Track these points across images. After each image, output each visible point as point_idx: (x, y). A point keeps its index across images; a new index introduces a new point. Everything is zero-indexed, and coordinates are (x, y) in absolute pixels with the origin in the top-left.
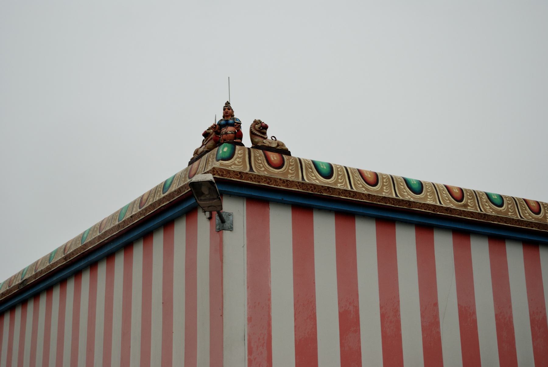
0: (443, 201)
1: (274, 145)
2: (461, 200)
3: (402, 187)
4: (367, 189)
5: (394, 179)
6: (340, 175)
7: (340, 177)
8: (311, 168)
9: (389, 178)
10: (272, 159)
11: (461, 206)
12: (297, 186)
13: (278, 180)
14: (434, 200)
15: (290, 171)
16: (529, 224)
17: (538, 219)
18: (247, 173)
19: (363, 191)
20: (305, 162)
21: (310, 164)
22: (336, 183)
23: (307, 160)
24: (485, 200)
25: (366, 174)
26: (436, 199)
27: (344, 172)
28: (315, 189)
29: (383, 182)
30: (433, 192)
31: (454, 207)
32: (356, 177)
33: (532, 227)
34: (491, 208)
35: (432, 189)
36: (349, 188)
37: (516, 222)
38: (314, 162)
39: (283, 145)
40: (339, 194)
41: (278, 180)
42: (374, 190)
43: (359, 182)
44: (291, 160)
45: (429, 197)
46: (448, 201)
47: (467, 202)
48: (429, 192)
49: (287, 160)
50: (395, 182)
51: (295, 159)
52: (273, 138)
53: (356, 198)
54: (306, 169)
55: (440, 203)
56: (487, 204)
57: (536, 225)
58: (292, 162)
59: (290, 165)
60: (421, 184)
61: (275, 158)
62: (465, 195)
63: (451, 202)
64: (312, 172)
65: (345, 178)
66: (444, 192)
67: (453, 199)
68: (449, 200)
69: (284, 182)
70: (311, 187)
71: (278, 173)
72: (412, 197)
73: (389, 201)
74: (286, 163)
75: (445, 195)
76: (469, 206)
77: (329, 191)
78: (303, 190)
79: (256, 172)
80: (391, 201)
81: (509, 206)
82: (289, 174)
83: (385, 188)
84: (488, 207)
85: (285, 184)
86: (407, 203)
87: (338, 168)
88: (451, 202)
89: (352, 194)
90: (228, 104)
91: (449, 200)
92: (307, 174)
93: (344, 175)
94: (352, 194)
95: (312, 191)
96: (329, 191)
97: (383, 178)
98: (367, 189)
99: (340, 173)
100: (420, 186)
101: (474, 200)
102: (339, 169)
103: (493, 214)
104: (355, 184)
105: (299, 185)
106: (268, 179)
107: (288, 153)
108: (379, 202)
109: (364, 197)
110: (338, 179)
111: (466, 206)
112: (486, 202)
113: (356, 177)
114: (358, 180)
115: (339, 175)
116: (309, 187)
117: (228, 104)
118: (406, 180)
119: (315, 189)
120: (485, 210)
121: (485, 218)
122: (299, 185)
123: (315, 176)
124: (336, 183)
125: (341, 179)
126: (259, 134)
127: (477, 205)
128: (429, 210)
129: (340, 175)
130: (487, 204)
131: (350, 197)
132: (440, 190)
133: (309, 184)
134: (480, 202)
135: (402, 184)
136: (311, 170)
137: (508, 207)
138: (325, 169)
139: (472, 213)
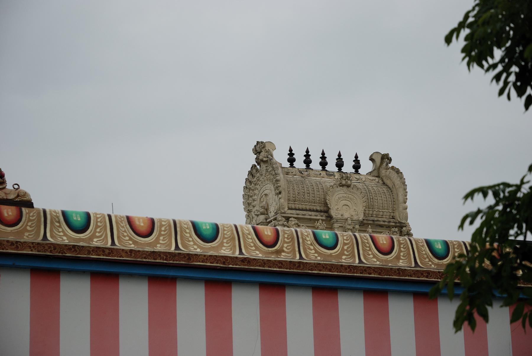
0: (246, 248)
3: (188, 235)
4: (135, 242)
5: (178, 225)
6: (99, 227)
7: (98, 230)
8: (59, 222)
9: (170, 225)
10: (6, 215)
11: (272, 253)
12: (30, 247)
13: (5, 243)
14: (233, 249)
15: (28, 228)
16: (365, 270)
18: (38, 244)
19: (259, 255)
20: (51, 214)
21: (58, 217)
22: (91, 239)
23: (55, 212)
24: (309, 243)
25: (137, 223)
26: (235, 246)
27: (105, 222)
28: (55, 249)
29: (161, 231)
30: (233, 238)
32: (123, 227)
33: (370, 274)
35: (233, 233)
37: (346, 269)
38: (64, 213)
39: (29, 195)
40: (89, 253)
41: (5, 243)
42: (146, 244)
43: (125, 234)
44: (31, 214)
45: (225, 244)
46: (254, 248)
47: (283, 247)
48: (226, 238)
49: (27, 213)
50: (178, 229)
51: (38, 211)
52: (16, 187)
53: (112, 256)
54: (52, 223)
56: (312, 247)
58: (33, 216)
59: (30, 220)
60: (216, 228)
61: (10, 213)
62: (280, 238)
63: (257, 248)
64: (60, 226)
65: (106, 230)
66: (250, 237)
67: (430, 254)
69: (12, 243)
70: (50, 247)
71: (11, 233)
72: (199, 247)
73: (160, 256)
74: (24, 219)
75: (251, 241)
76: (284, 251)
77: (75, 251)
78: (38, 251)
79: (246, 255)
80: (162, 255)
81: (346, 247)
82: (27, 233)
83: (402, 254)
84: (192, 243)
85: (13, 247)
86: (185, 257)
87: (97, 218)
88: (257, 248)
89: (107, 251)
90: (340, 152)
92: (51, 231)
93: (105, 226)
94: (107, 251)
95: (51, 252)
96: (75, 251)
97: (161, 226)
98: (135, 242)
99: (99, 224)
100: (335, 237)
101: (294, 243)
102: (99, 220)
104: (118, 237)
105: (34, 247)
106: (73, 248)
107: (29, 204)
108: (145, 258)
109: (123, 254)
110: (95, 232)
111: (21, 233)
112: (311, 244)
113: (123, 227)
114: (125, 231)
116: (47, 248)
117: (340, 152)
118: (194, 225)
119: (55, 249)
120: (307, 255)
121: (299, 266)
122: (34, 247)
123: (63, 231)
125: (99, 232)
127: (297, 249)
128: (217, 263)
129: (99, 227)
130: (312, 247)
131: (104, 255)
132: (243, 234)
133: (52, 244)
134: (301, 245)
135: (188, 231)
136: (58, 224)
137: (343, 247)
138: (77, 220)
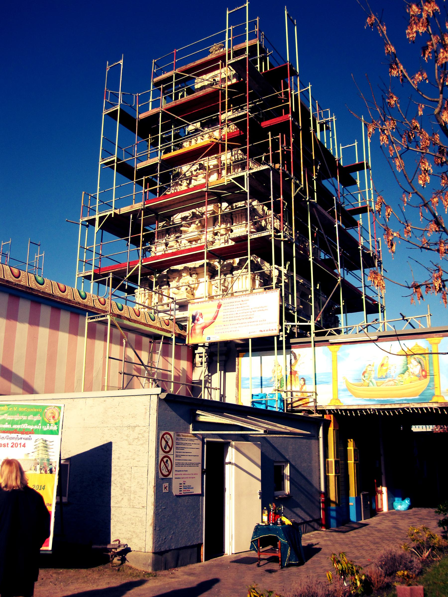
1: (276, 407)
2: (18, 277)
4: (37, 286)
11: (17, 281)
17: (63, 295)
31: (12, 281)
34: (35, 285)
36: (3, 277)
55: (4, 277)
57: (60, 298)
59: (23, 278)
63: (99, 306)
68: (10, 276)
88: (11, 277)
91: (10, 276)
103: (36, 288)
115: (47, 284)
124: (67, 295)
126: (283, 295)
139: (22, 286)
